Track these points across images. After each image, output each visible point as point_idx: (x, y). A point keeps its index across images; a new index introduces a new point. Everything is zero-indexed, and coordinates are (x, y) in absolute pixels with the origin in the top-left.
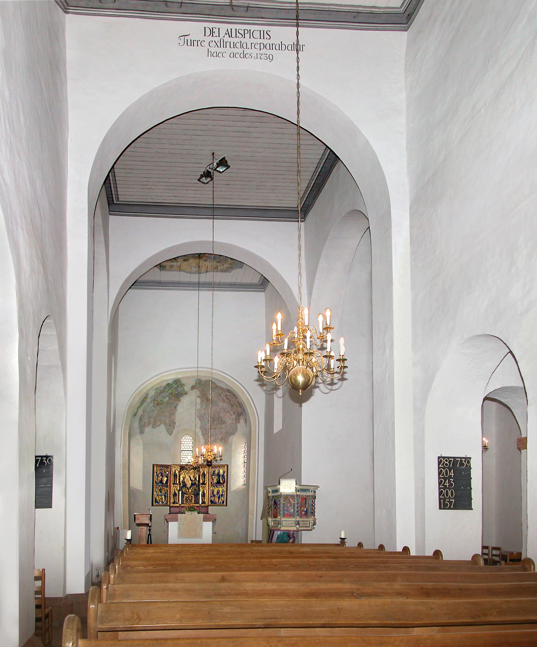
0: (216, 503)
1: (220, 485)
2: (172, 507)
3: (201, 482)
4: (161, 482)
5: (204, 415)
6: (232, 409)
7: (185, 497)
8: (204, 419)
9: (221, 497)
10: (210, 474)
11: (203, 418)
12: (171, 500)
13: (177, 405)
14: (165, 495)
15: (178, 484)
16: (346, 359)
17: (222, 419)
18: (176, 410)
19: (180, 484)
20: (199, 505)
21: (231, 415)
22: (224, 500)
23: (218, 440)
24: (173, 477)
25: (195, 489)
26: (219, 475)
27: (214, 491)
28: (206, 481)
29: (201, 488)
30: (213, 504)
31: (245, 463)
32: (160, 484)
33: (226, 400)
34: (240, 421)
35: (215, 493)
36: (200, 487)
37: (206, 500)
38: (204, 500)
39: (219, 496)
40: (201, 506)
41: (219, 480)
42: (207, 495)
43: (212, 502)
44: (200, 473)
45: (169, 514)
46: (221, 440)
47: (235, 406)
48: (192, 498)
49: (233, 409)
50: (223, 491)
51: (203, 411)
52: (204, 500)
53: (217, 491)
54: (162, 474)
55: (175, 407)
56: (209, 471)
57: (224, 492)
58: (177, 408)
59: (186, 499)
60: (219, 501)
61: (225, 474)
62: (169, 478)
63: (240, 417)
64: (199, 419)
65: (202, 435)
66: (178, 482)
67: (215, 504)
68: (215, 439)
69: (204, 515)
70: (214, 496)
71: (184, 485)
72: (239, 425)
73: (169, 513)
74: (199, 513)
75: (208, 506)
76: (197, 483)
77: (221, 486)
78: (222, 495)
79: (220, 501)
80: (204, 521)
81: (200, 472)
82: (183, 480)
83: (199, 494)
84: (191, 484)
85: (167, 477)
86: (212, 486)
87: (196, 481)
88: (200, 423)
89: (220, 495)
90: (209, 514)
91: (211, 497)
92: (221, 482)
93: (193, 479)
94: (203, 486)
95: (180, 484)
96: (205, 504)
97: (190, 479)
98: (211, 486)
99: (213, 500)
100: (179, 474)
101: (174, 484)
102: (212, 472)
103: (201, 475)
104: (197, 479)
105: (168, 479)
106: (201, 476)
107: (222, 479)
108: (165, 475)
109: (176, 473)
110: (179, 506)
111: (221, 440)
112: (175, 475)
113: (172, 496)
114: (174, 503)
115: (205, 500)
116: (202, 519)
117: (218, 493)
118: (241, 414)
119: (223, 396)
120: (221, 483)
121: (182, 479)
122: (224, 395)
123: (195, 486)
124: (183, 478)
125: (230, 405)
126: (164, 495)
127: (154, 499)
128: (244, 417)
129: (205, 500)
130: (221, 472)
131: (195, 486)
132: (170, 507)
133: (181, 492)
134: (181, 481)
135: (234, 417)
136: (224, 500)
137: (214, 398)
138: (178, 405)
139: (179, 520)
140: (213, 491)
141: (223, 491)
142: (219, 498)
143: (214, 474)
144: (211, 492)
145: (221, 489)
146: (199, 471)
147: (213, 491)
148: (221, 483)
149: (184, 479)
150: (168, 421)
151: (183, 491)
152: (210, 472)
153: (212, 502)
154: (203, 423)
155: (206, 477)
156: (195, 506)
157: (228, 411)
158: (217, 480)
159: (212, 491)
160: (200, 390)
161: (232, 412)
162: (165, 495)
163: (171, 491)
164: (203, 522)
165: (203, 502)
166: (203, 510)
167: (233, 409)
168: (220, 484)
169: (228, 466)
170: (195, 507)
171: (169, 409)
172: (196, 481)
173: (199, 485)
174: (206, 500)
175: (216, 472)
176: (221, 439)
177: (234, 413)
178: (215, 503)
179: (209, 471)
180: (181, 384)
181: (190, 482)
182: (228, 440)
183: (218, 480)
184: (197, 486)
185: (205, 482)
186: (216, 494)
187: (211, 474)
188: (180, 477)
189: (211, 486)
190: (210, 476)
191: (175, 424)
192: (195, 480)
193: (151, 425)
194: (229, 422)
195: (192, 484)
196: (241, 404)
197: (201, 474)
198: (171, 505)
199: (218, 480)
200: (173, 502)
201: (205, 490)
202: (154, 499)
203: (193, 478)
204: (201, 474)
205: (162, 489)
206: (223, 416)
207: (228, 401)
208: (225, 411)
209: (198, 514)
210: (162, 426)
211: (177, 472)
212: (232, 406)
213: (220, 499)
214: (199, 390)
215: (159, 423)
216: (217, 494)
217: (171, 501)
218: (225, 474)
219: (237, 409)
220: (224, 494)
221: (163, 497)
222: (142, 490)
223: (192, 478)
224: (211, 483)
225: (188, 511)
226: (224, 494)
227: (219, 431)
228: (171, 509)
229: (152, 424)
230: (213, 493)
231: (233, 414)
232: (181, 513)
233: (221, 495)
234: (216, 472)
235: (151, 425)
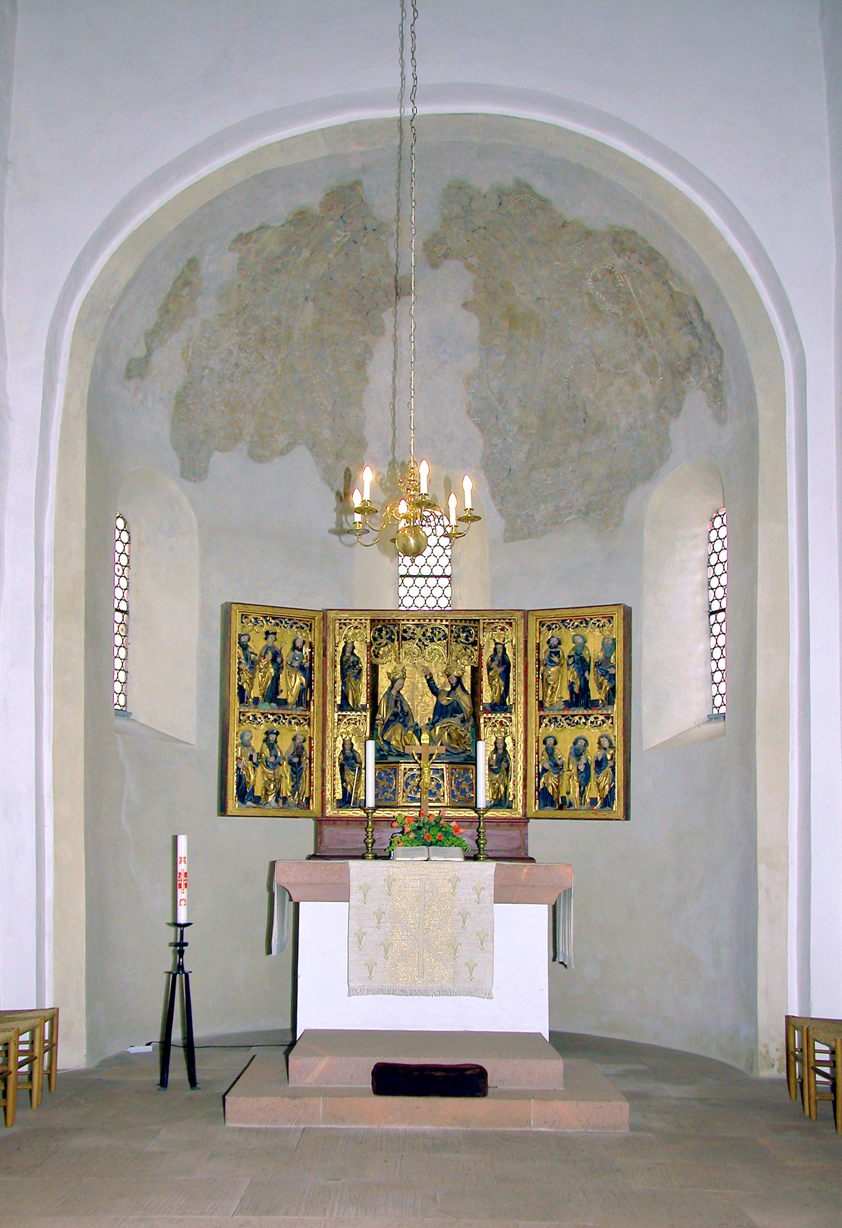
0: (571, 805)
1: (590, 712)
2: (334, 821)
3: (487, 697)
4: (273, 694)
5: (500, 401)
6: (641, 349)
7: (401, 773)
8: (501, 423)
9: (593, 772)
10: (532, 661)
11: (494, 420)
12: (328, 786)
13: (368, 351)
14: (296, 760)
15: (364, 708)
16: (534, 859)
17: (590, 412)
18: (366, 380)
19: (375, 709)
20: (361, 813)
21: (635, 385)
22: (612, 790)
23: (570, 514)
24: (338, 675)
25: (454, 735)
26: (581, 663)
27: (555, 743)
28: (516, 696)
29: (485, 731)
30: (549, 811)
31: (712, 613)
32: (266, 707)
33: (607, 307)
34: (686, 405)
35: (563, 751)
36: (482, 721)
37: (515, 790)
38: (502, 788)
39: (582, 768)
40: (376, 821)
41: (585, 688)
42: (521, 764)
43: (546, 798)
44: (480, 655)
45: (310, 857)
46: (587, 514)
47: (657, 325)
48: (442, 777)
49: (645, 345)
50: (606, 743)
51: (494, 384)
52: (502, 788)
53: (575, 743)
54: (276, 655)
55: (361, 365)
56: (526, 642)
57: (611, 746)
58: (370, 369)
59: (407, 784)
60: (582, 794)
61: (617, 657)
62: (317, 676)
63: (684, 383)
64: (478, 425)
65: (494, 497)
66: (363, 700)
67: (561, 808)
68: (557, 510)
69: (497, 864)
70: (557, 767)
71: (395, 715)
72: (677, 429)
73: (312, 853)
74: (475, 858)
75: (525, 819)
76: (465, 702)
77: (592, 719)
78: (600, 764)
79: (592, 792)
80: (499, 898)
81: (481, 649)
82: (391, 688)
83: (472, 760)
84: (432, 708)
85: (307, 671)
86: (546, 721)
87: (459, 691)
88: (480, 442)
89: (587, 766)
90: (532, 860)
91: (539, 776)
92: (595, 694)
93: (445, 685)
94: (500, 717)
95: (375, 709)
96: (510, 807)
97: (430, 681)
98: (542, 718)
99: (550, 790)
100: (370, 662)
101: (344, 706)
102: (545, 647)
103: (484, 664)
104: (467, 685)
105: (310, 682)
106: (484, 671)
107: (597, 680)
108: (296, 664)
109: (355, 652)
110: (366, 820)
111: (586, 513)
112: (349, 667)
113: (333, 772)
114: (346, 801)
115: (506, 788)
116: (489, 893)
117: (578, 754)
118: (689, 361)
119: (590, 283)
120: (590, 704)
121: (384, 684)
122: (595, 279)
123: (455, 721)
124: (393, 682)
125: (631, 329)
126: (290, 763)
127: (232, 779)
128: (706, 373)
129: (510, 790)
130: (594, 650)
131: (452, 720)
132: (321, 821)
133: (378, 750)
134: (380, 697)
135: (647, 390)
136: (612, 790)
137: (547, 303)
138: (371, 354)
139: (356, 895)
140: (550, 741)
141: (606, 743)
142: (584, 779)
143: (555, 659)
144: (542, 747)
145: (592, 735)
146: (474, 644)
147: (550, 741)
148: (590, 704)
149: (397, 685)
150: (327, 434)
151: (393, 743)
152: (532, 647)
153: (546, 798)
154: (496, 440)
155: (511, 675)
156: (450, 820)
157: (616, 367)
158: (571, 686)
159: (545, 742)
160: (474, 261)
161: (638, 368)
162: (296, 760)
163: (329, 741)
164: (501, 909)
165: (501, 801)
166: (494, 840)
167: (645, 345)
168: (587, 707)
169: (627, 614)
170: (454, 824)
171: (331, 374)
172: (459, 691)
173: (475, 716)
174: (516, 790)
175: (567, 649)
176: (583, 509)
177: (651, 368)
178: (564, 805)
179: (526, 642)
180: (369, 222)
181: (431, 700)
182: (622, 509)
183: (576, 690)
184: (463, 721)
185: (510, 701)
186: (565, 760)
187: (538, 660)
188: (374, 670)
189: (542, 718)
190: (532, 666)
191: (366, 448)
192: (453, 688)
193: (243, 446)
194: (624, 423)
195: (441, 712)
196: (691, 308)
197: (486, 659)
198: (330, 812)
199: (576, 690)
200: (339, 796)
201: (508, 740)
202: (232, 779)
203: (443, 680)
204: (486, 659)
205: (277, 734)
206: (591, 396)
207: (616, 309)
208: (601, 370)
209: (467, 858)
210: (302, 454)
211: (361, 651)
212: (641, 332)
213: (592, 783)
214: (468, 267)
215: (282, 440)
216: (573, 759)
217: (328, 794)
218: (617, 657)
219: (668, 343)
220: (609, 757)
221: (285, 770)
222: (193, 740)
223: (440, 681)
224: (541, 705)
225: (411, 843)
226: (609, 757)
227: (573, 471)
228: (327, 830)
229: (248, 439)
230: (551, 753)
231: (644, 375)
232: (376, 857)
233: (593, 766)
234: (567, 649)
235: (243, 446)
